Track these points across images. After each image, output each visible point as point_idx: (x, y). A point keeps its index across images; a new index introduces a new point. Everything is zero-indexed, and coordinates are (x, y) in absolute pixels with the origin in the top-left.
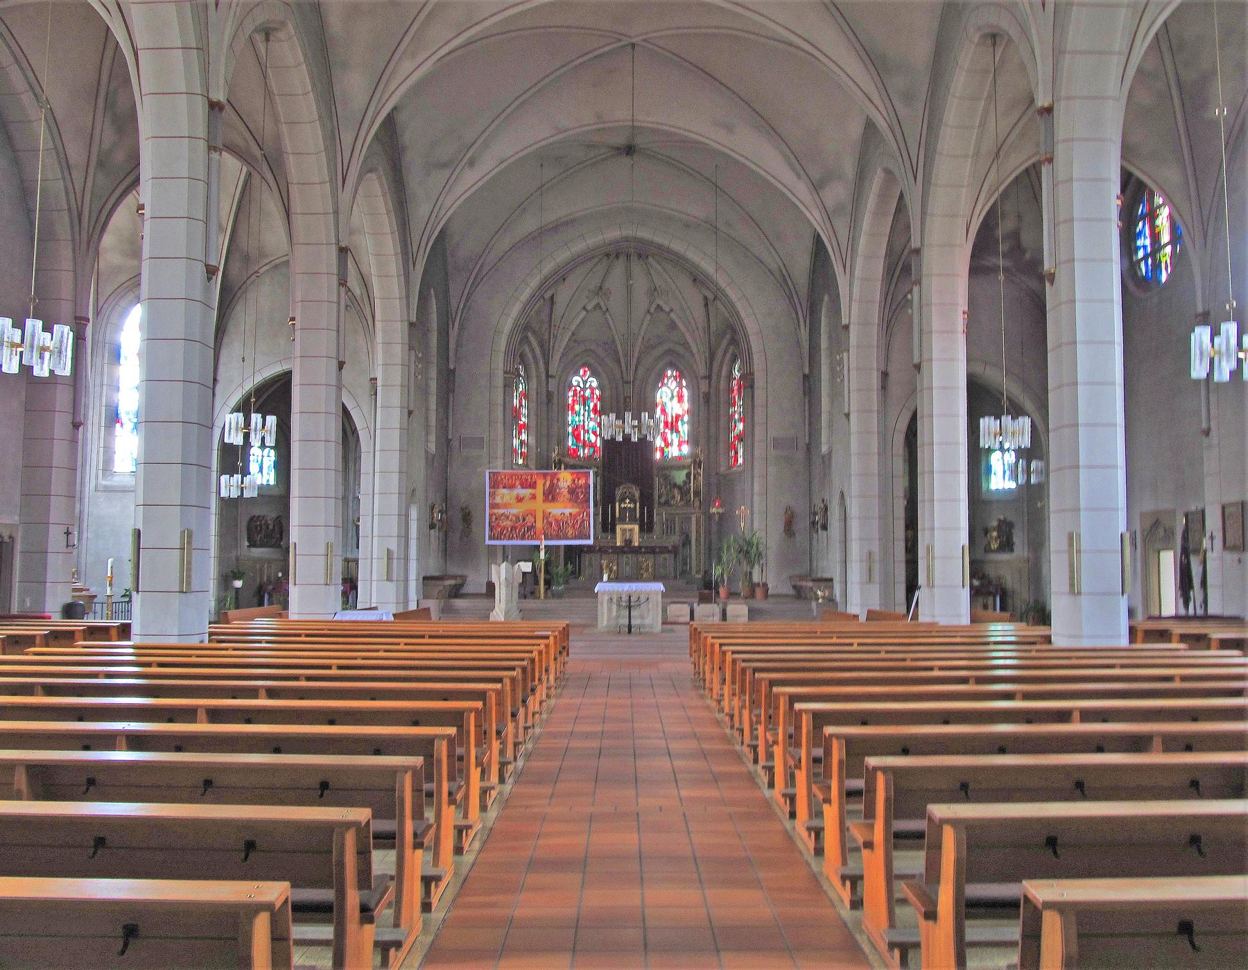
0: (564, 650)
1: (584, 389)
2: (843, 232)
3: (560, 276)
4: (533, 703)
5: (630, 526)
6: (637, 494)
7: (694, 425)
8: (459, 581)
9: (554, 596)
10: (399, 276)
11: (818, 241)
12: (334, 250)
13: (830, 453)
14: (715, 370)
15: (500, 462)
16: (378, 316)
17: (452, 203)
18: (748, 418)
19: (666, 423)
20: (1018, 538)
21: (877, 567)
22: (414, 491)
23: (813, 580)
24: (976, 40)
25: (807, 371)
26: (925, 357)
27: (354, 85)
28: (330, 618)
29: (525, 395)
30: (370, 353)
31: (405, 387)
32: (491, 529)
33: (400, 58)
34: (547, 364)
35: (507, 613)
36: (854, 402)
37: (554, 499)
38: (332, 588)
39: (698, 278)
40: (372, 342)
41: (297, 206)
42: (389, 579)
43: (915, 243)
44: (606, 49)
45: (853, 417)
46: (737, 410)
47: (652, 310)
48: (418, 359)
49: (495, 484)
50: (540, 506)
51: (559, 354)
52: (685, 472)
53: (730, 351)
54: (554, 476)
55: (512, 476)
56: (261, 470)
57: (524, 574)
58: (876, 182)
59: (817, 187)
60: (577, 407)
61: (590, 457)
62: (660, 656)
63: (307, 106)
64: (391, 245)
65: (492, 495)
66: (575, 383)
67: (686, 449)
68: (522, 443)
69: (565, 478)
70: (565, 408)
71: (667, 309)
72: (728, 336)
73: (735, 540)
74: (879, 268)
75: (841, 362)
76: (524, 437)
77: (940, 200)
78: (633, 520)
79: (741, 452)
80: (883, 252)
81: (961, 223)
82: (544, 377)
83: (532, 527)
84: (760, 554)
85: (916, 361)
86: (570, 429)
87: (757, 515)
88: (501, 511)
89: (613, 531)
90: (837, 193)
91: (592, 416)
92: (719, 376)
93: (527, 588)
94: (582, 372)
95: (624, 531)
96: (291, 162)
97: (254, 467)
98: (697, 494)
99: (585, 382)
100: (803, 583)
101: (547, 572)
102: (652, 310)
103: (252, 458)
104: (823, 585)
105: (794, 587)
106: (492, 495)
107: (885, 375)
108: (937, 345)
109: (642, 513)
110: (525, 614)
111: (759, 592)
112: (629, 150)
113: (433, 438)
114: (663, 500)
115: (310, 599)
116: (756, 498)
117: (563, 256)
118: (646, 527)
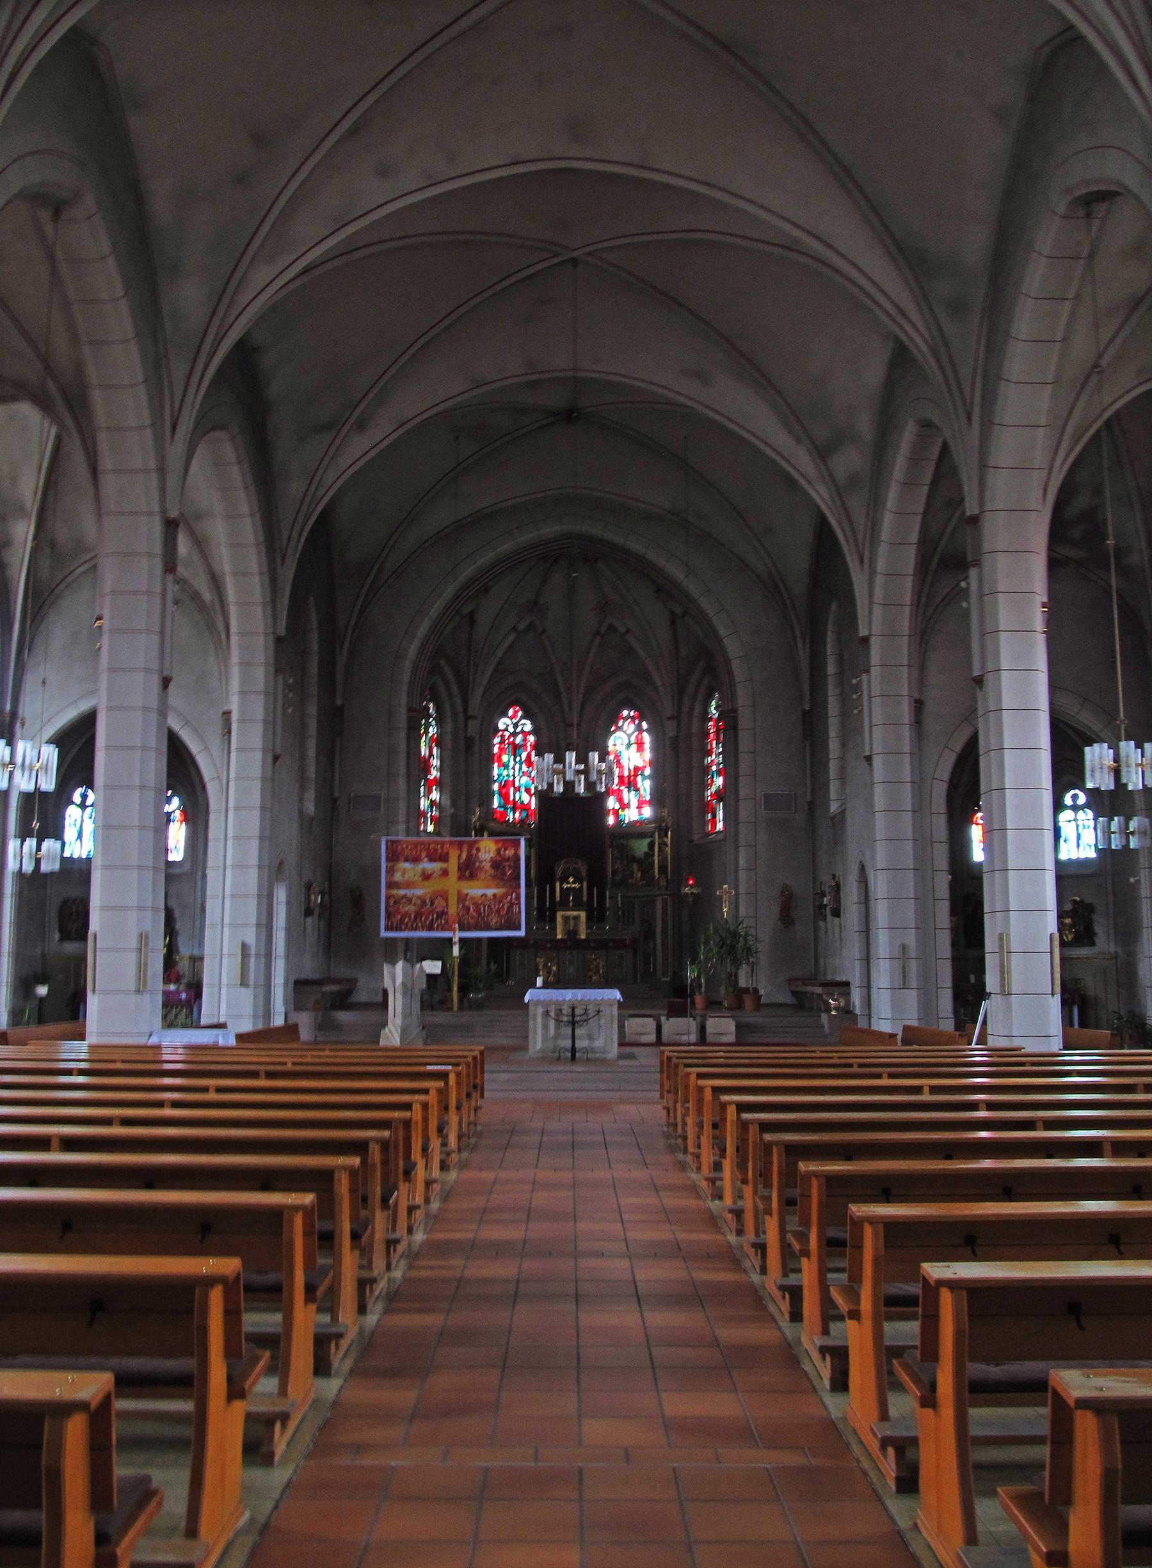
0: (478, 1088)
1: (514, 734)
2: (860, 520)
3: (480, 586)
4: (402, 1196)
5: (575, 913)
6: (584, 872)
7: (656, 777)
8: (345, 987)
9: (470, 1008)
10: (261, 574)
11: (823, 528)
12: (157, 526)
13: (843, 812)
14: (685, 708)
15: (402, 827)
16: (234, 628)
17: (334, 478)
18: (730, 770)
19: (621, 778)
20: (1101, 928)
21: (913, 965)
22: (281, 864)
23: (823, 985)
24: (1061, 209)
25: (807, 707)
26: (990, 667)
27: (189, 296)
28: (142, 1041)
29: (438, 741)
30: (225, 677)
31: (269, 723)
32: (389, 916)
33: (252, 260)
34: (465, 702)
35: (404, 1032)
36: (877, 739)
37: (472, 877)
38: (147, 997)
39: (664, 588)
40: (226, 667)
41: (106, 462)
42: (244, 983)
43: (971, 509)
44: (539, 267)
45: (877, 762)
46: (714, 760)
47: (602, 630)
48: (289, 688)
49: (394, 856)
50: (453, 885)
51: (481, 690)
52: (649, 840)
53: (706, 682)
54: (472, 845)
55: (416, 845)
56: (80, 836)
57: (431, 977)
58: (908, 434)
59: (823, 453)
60: (505, 758)
61: (522, 821)
62: (617, 1094)
63: (118, 320)
64: (249, 530)
65: (391, 871)
66: (501, 726)
67: (647, 812)
68: (433, 803)
69: (487, 848)
70: (490, 759)
71: (623, 630)
72: (702, 664)
73: (716, 931)
74: (909, 559)
75: (857, 689)
76: (435, 795)
77: (1007, 446)
78: (578, 906)
79: (720, 815)
80: (914, 538)
81: (1037, 478)
82: (461, 716)
83: (442, 914)
84: (749, 949)
85: (976, 673)
86: (496, 787)
87: (742, 899)
88: (402, 892)
89: (553, 920)
90: (850, 460)
91: (525, 768)
92: (690, 716)
93: (433, 994)
94: (511, 712)
95: (566, 919)
96: (97, 398)
97: (70, 833)
98: (663, 869)
99: (516, 726)
100: (809, 989)
101: (462, 974)
102: (602, 630)
103: (67, 823)
104: (836, 991)
105: (795, 994)
106: (391, 871)
107: (918, 705)
108: (1007, 651)
109: (590, 895)
110: (431, 1033)
111: (748, 1002)
112: (570, 415)
113: (311, 795)
114: (617, 878)
115: (119, 1011)
116: (742, 876)
117: (486, 558)
118: (596, 916)
